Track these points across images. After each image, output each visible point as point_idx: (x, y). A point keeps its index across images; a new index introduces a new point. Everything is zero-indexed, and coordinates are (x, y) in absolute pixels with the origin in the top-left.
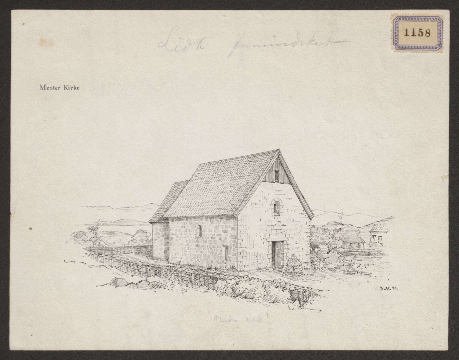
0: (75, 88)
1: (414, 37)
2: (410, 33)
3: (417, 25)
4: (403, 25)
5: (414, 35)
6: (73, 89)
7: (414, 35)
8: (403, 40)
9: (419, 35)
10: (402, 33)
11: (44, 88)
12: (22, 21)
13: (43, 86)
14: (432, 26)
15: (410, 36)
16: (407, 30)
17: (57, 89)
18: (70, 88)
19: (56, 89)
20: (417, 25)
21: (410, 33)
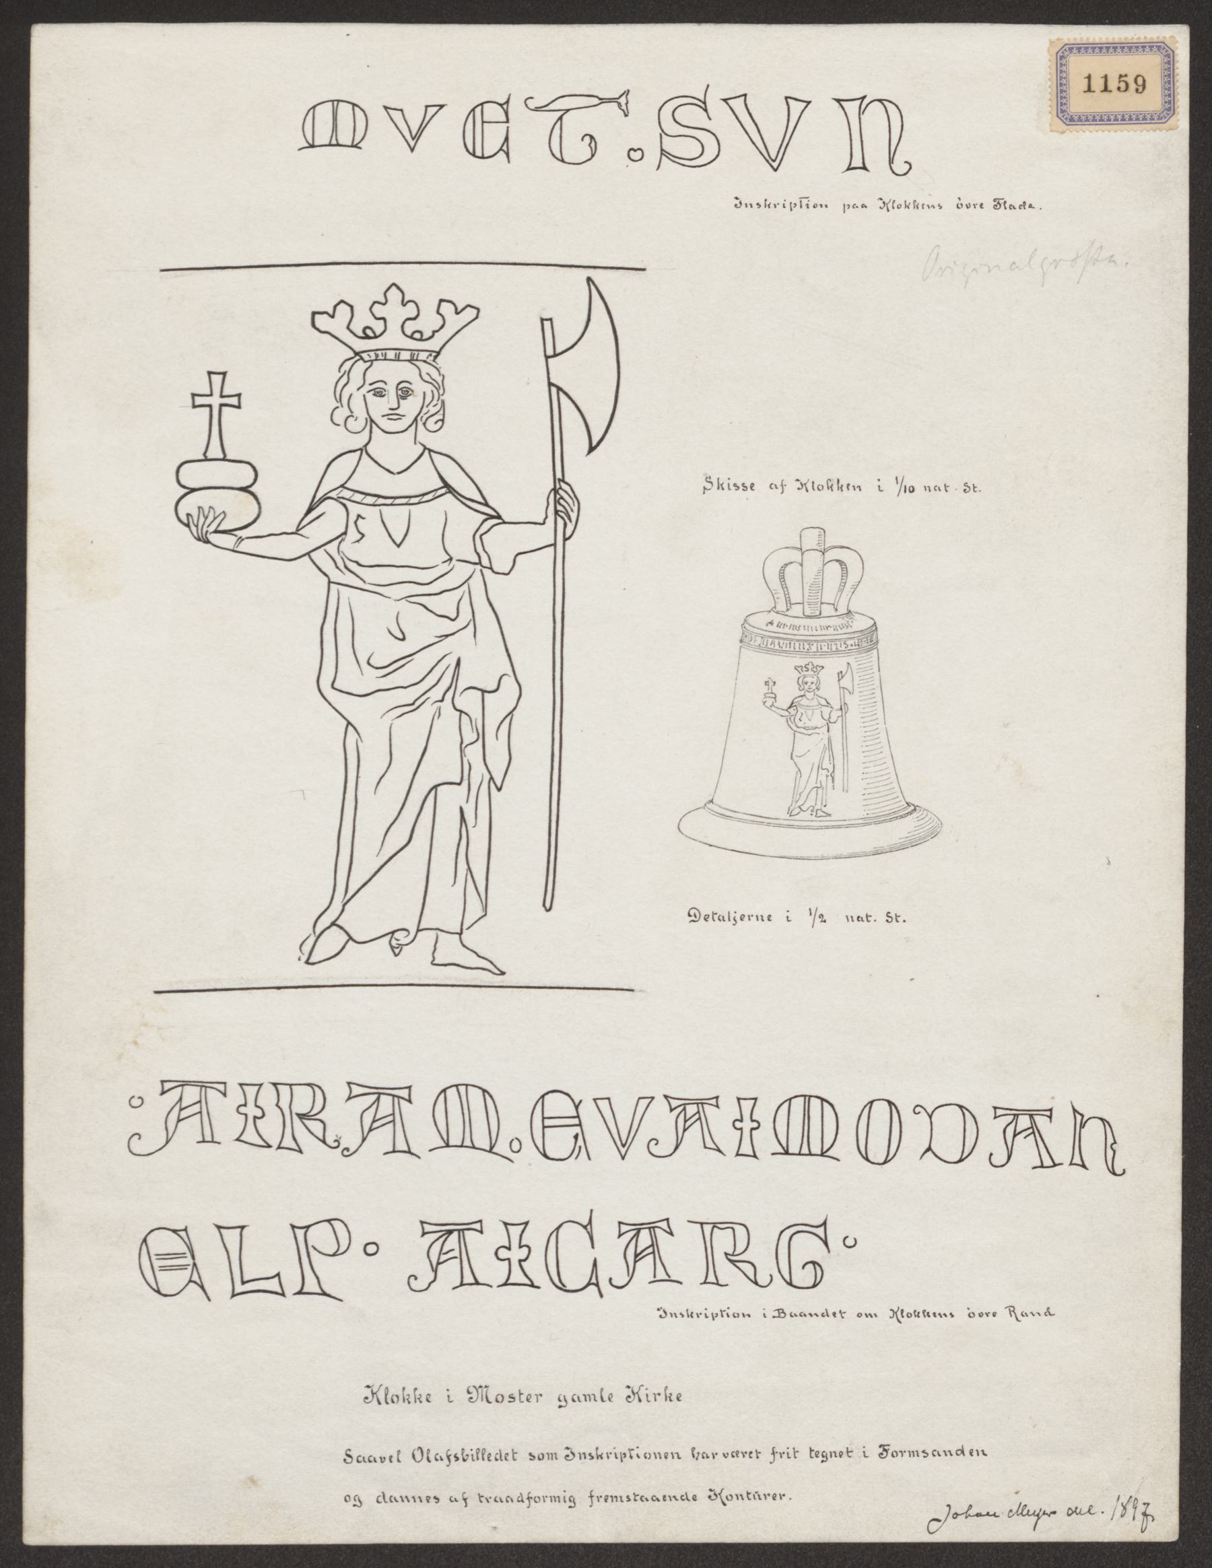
0: (668, 1398)
1: (1089, 94)
2: (1097, 84)
3: (1115, 65)
4: (1079, 66)
5: (1106, 89)
6: (661, 1399)
7: (1106, 89)
8: (1079, 103)
9: (1119, 89)
10: (1077, 84)
11: (694, 916)
12: (55, 47)
13: (900, 480)
14: (1149, 65)
15: (1115, 91)
16: (1106, 77)
17: (533, 1399)
18: (651, 1398)
19: (971, 1454)
20: (1115, 65)
21: (1097, 84)
